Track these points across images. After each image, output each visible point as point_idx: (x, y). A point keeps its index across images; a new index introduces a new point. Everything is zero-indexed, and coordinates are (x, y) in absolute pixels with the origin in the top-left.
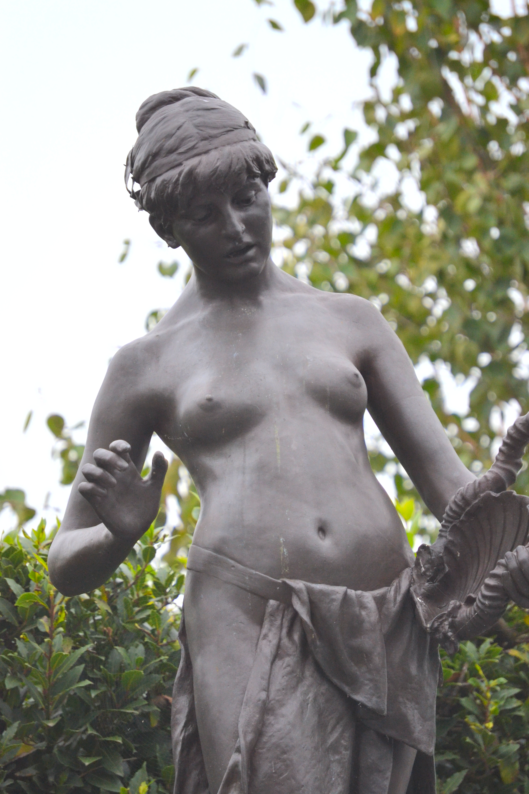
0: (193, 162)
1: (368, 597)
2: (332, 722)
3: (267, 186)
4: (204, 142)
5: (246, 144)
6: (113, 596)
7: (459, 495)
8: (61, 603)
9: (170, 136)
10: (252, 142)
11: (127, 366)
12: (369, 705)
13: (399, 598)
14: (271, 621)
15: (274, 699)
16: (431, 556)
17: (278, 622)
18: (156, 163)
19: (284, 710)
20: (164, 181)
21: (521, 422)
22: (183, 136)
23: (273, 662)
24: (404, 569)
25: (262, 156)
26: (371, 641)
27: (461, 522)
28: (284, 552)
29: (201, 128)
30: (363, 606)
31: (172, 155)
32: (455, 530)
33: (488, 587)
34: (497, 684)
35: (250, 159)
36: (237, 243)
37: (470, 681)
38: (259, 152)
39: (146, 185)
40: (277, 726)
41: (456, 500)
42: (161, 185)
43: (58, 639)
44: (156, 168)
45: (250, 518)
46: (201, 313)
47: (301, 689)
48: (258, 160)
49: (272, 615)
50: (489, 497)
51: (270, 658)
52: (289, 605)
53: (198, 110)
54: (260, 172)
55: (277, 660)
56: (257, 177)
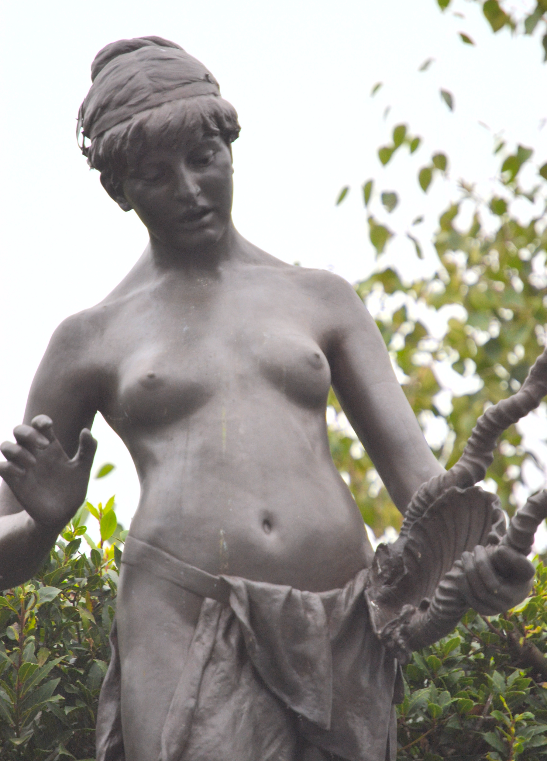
0: (144, 115)
1: (316, 599)
2: (269, 736)
3: (228, 145)
4: (157, 95)
5: (205, 99)
6: (99, 605)
7: (423, 490)
8: (32, 608)
9: (120, 87)
10: (212, 98)
11: (70, 337)
12: (311, 717)
13: (351, 602)
14: (206, 621)
15: (204, 708)
16: (389, 556)
17: (214, 623)
18: (105, 116)
19: (214, 721)
20: (111, 136)
21: (491, 411)
22: (134, 88)
23: (205, 667)
24: (360, 569)
25: (222, 112)
26: (317, 648)
27: (424, 520)
28: (223, 546)
29: (154, 79)
30: (309, 608)
31: (122, 107)
32: (418, 528)
33: (444, 591)
34: (522, 718)
35: (208, 114)
36: (191, 207)
37: (494, 714)
38: (218, 107)
39: (95, 140)
40: (205, 738)
41: (420, 496)
42: (108, 140)
43: (30, 648)
44: (104, 121)
45: (190, 507)
46: (154, 283)
47: (236, 697)
48: (217, 116)
49: (207, 615)
50: (454, 492)
51: (202, 662)
52: (226, 605)
53: (153, 59)
54: (218, 129)
55: (210, 664)
56: (216, 135)
